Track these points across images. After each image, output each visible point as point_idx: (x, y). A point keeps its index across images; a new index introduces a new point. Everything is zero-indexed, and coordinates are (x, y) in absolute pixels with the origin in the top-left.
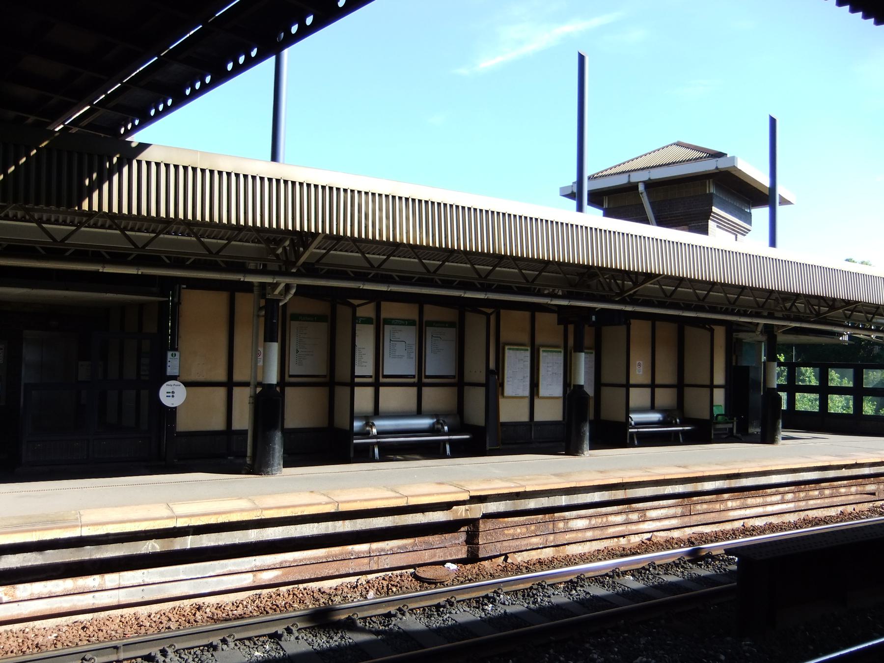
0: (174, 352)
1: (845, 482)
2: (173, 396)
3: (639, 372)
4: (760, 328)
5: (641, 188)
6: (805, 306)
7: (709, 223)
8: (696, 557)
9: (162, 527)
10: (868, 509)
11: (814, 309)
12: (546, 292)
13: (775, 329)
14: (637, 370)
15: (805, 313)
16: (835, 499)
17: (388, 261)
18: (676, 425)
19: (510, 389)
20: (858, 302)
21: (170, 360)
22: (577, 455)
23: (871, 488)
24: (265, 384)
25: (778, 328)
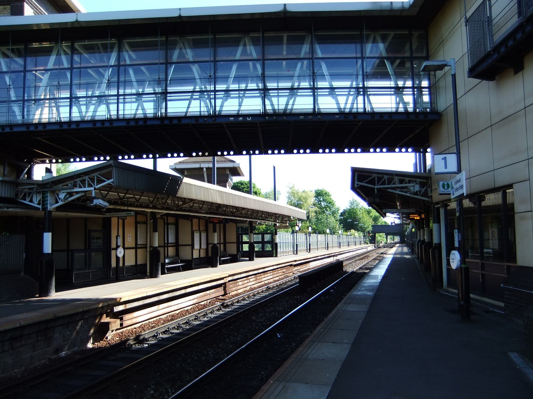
1: (280, 269)
4: (248, 222)
5: (205, 170)
6: (172, 202)
8: (268, 289)
9: (217, 278)
11: (176, 203)
12: (26, 190)
13: (157, 214)
15: (171, 205)
16: (278, 274)
17: (108, 195)
18: (178, 263)
19: (195, 248)
20: (196, 200)
23: (284, 270)
24: (154, 247)
25: (158, 214)
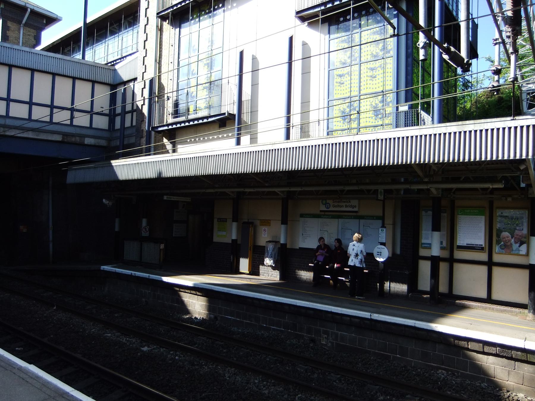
0: (382, 229)
2: (381, 255)
3: (264, 235)
7: (126, 127)
10: (182, 107)
14: (263, 234)
21: (380, 233)
22: (6, 42)
